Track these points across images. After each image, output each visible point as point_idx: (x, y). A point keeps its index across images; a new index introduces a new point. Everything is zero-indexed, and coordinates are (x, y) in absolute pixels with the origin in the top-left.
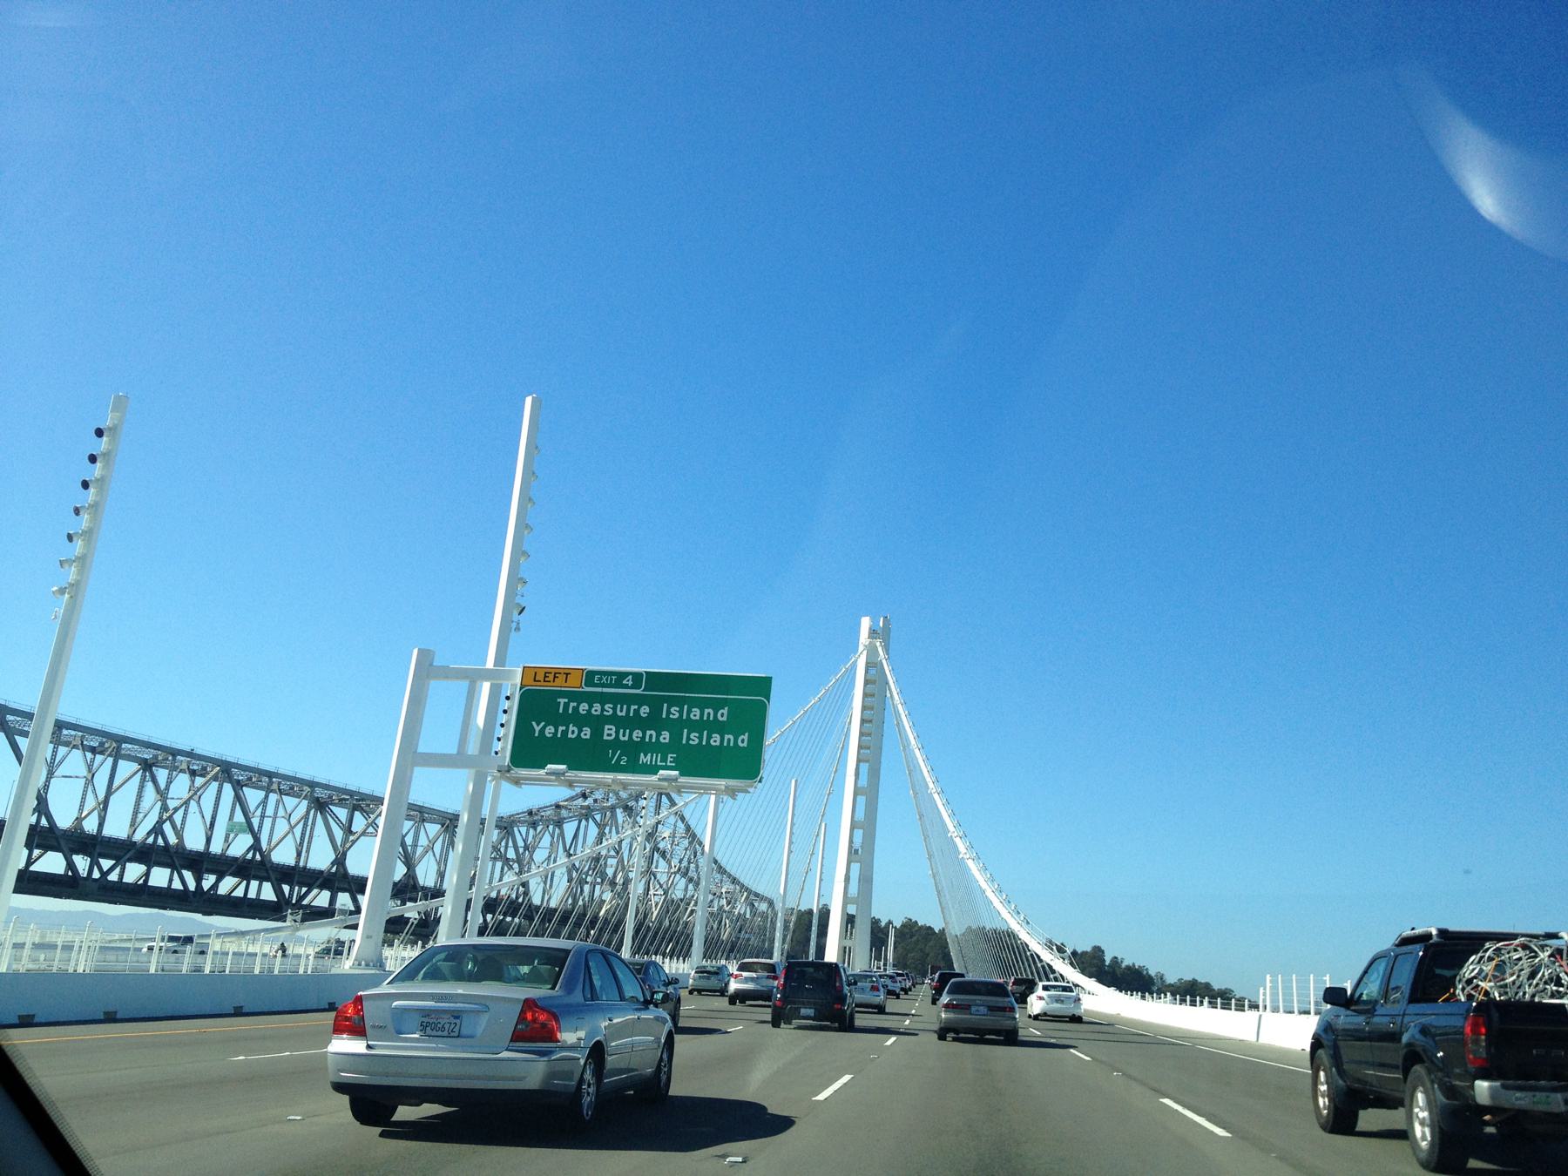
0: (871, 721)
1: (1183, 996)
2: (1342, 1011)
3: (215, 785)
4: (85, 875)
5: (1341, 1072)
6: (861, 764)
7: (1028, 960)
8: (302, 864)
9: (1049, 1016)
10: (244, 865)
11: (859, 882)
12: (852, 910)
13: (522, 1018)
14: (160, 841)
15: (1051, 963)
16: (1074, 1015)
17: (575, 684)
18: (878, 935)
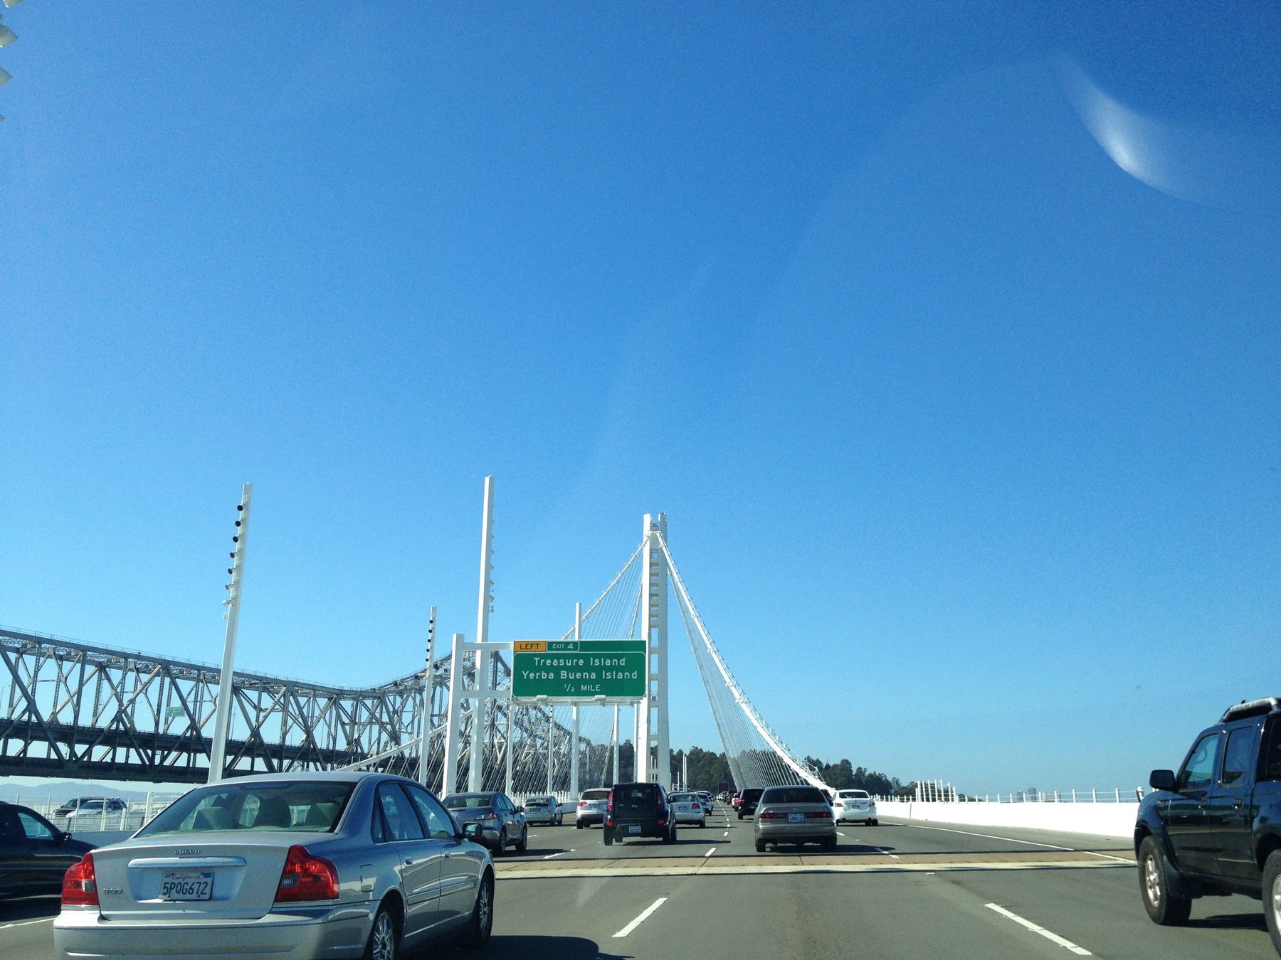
0: (657, 595)
1: (902, 795)
2: (1170, 795)
3: (158, 680)
4: (68, 758)
5: (1173, 860)
7: (790, 776)
9: (848, 821)
10: (109, 734)
12: (654, 744)
14: (34, 719)
15: (807, 779)
16: (870, 819)
17: (543, 650)
18: (675, 762)
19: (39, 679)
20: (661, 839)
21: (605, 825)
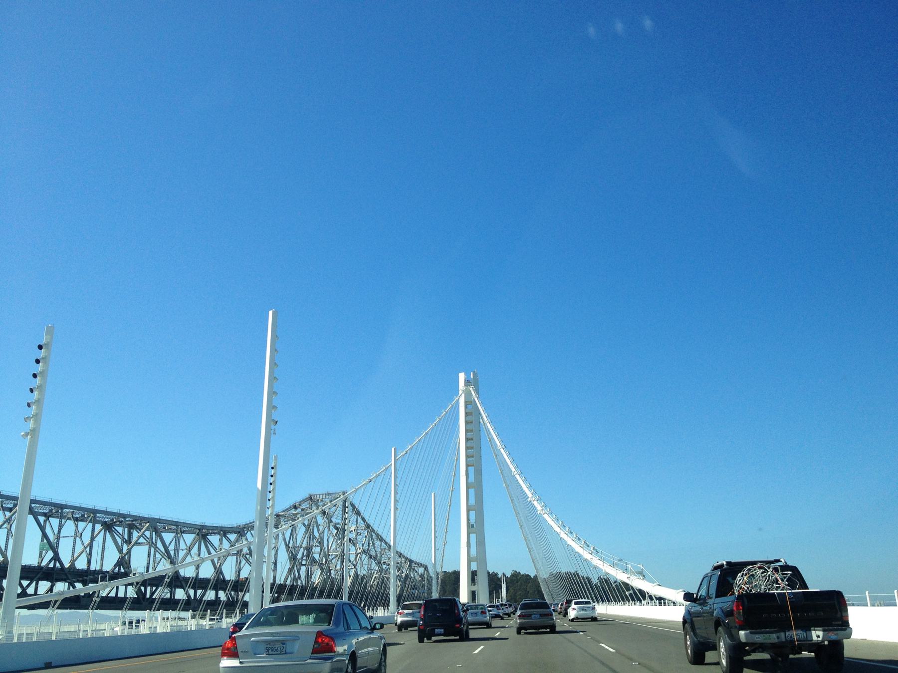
2: (693, 604)
6: (469, 468)
9: (579, 619)
12: (474, 567)
13: (316, 642)
16: (592, 617)
18: (494, 582)
19: (62, 535)
20: (458, 637)
21: (419, 628)
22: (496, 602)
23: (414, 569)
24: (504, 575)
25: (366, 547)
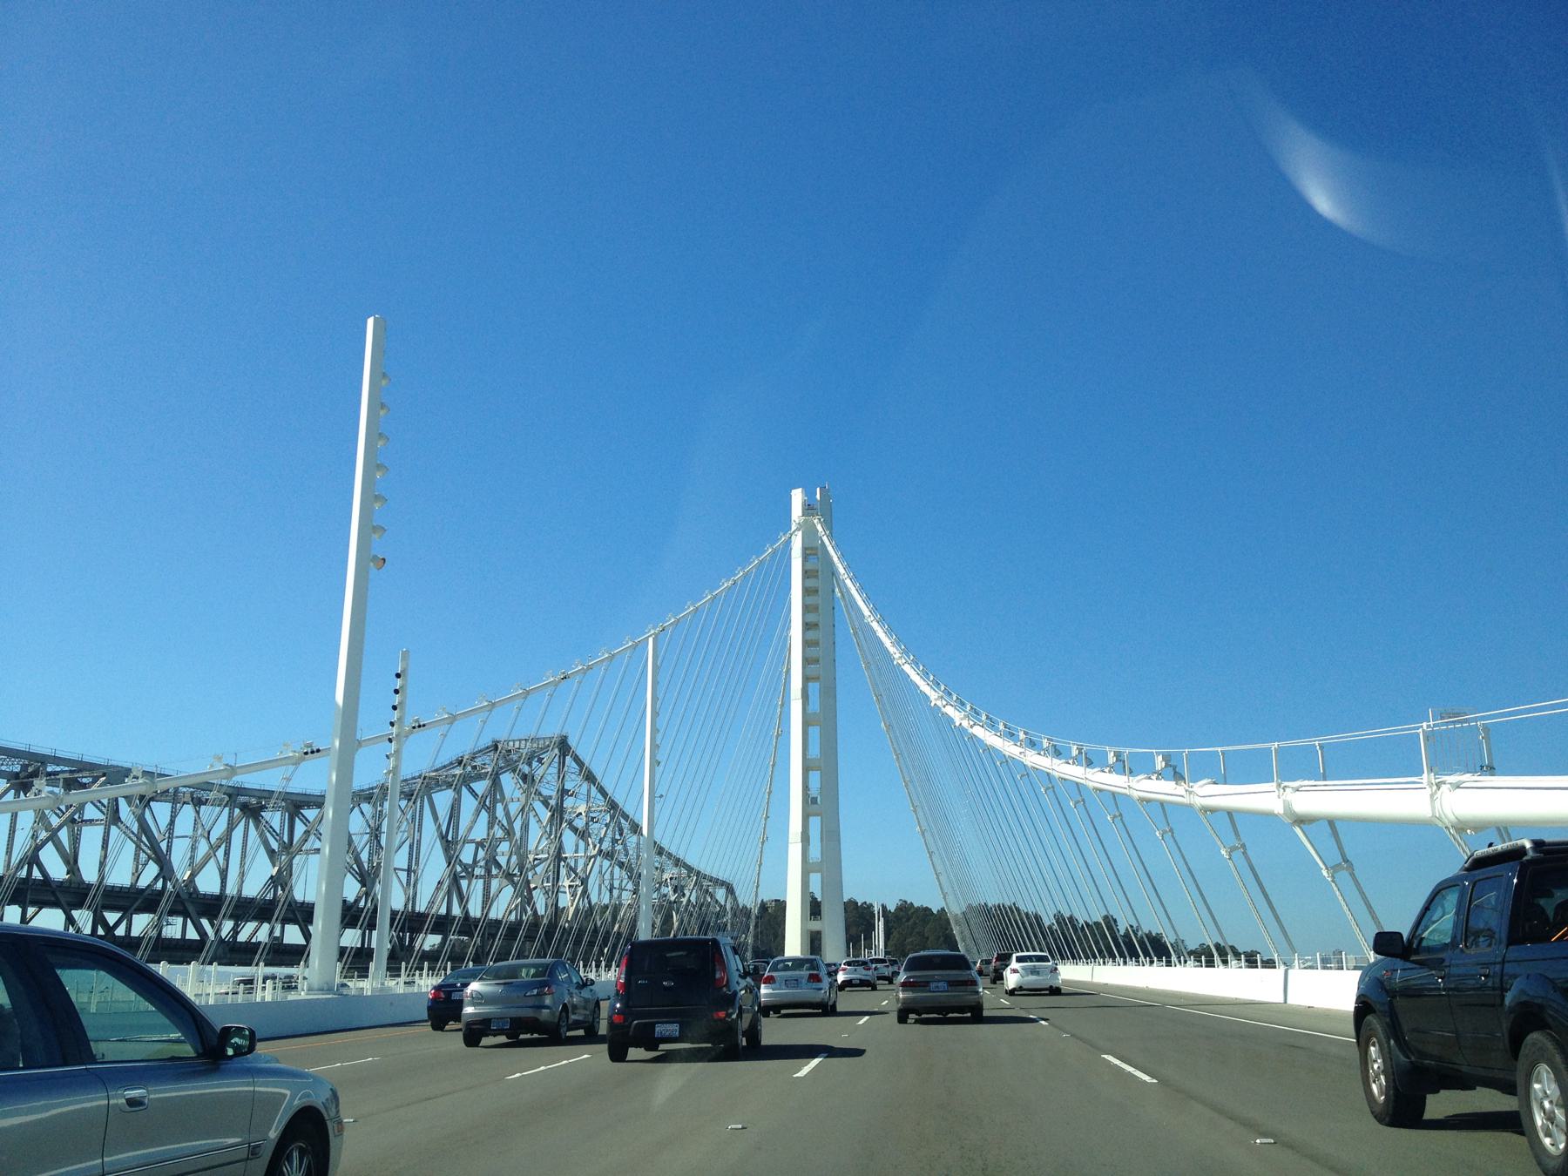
2: (1399, 963)
5: (1403, 1046)
6: (810, 684)
8: (417, 910)
9: (1025, 990)
11: (822, 841)
14: (36, 874)
16: (1051, 987)
18: (859, 919)
22: (865, 955)
23: (707, 890)
24: (884, 907)
25: (606, 845)
